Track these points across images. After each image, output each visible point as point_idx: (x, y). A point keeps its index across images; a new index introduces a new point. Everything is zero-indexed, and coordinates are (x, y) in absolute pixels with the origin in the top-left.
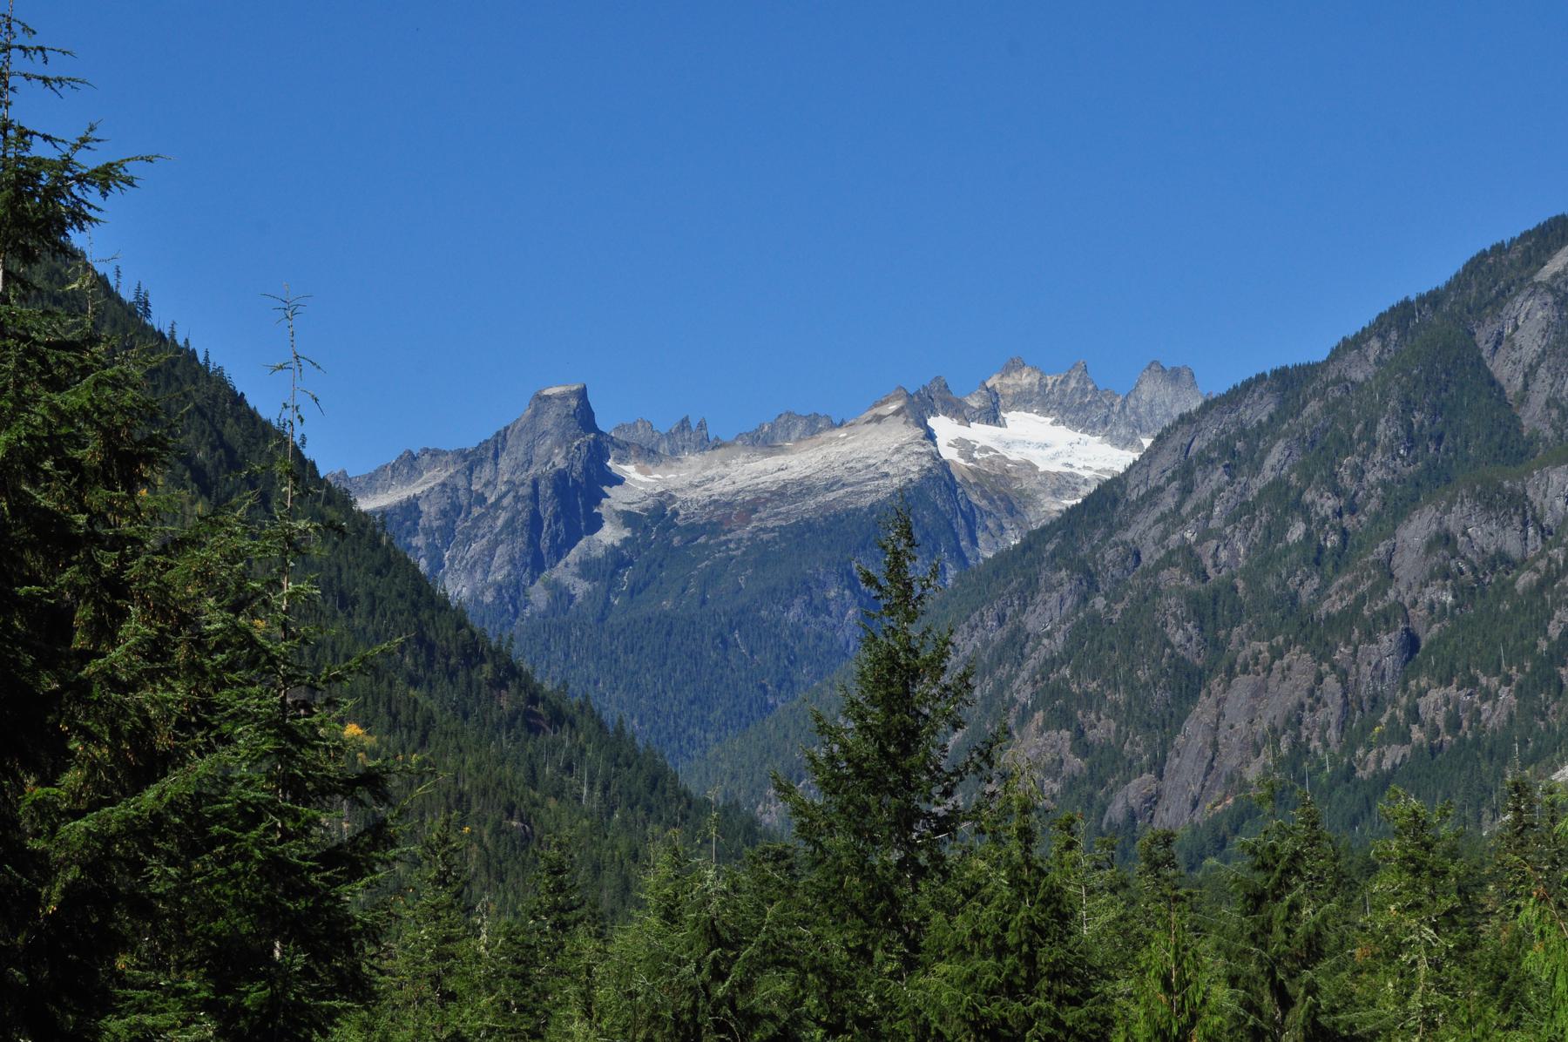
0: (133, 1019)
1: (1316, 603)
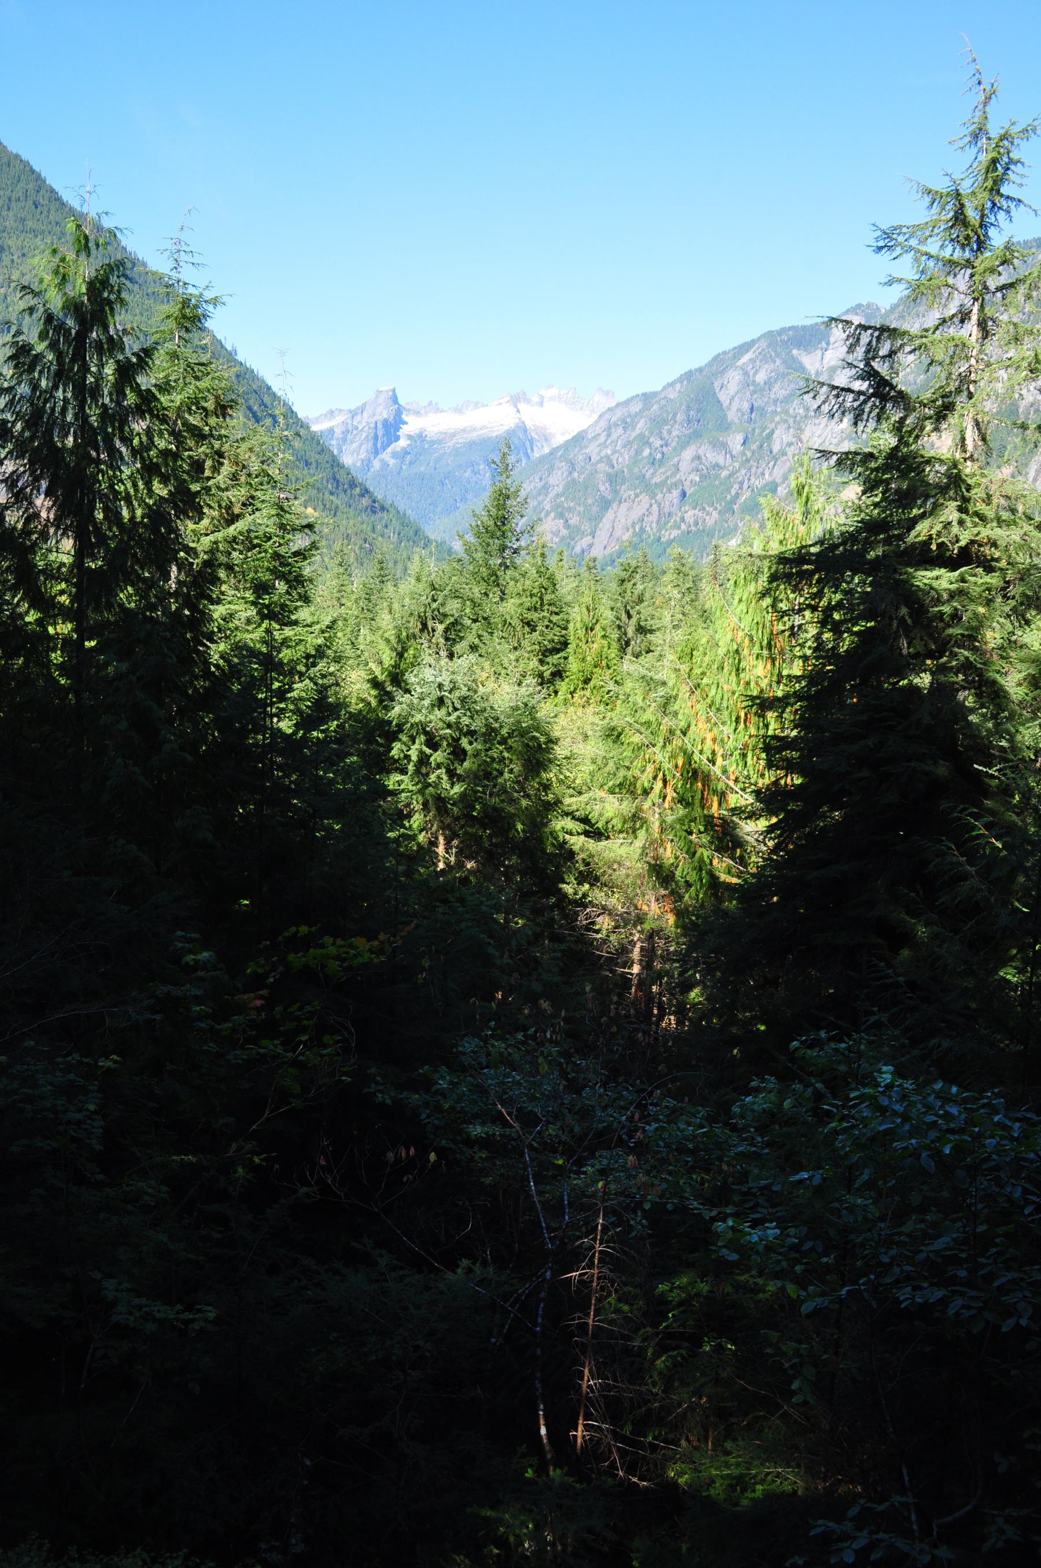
0: (227, 606)
1: (652, 478)
